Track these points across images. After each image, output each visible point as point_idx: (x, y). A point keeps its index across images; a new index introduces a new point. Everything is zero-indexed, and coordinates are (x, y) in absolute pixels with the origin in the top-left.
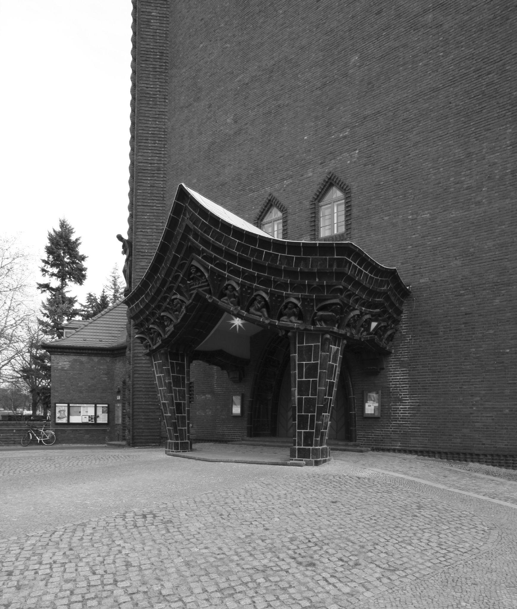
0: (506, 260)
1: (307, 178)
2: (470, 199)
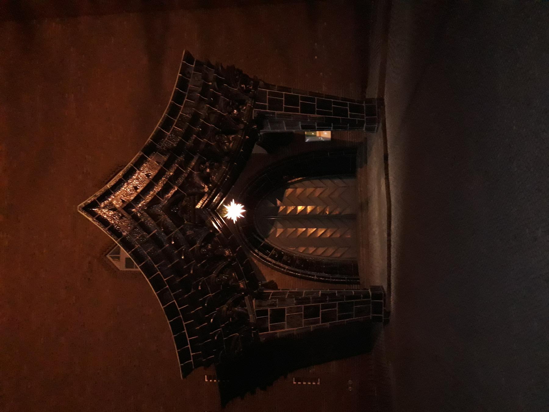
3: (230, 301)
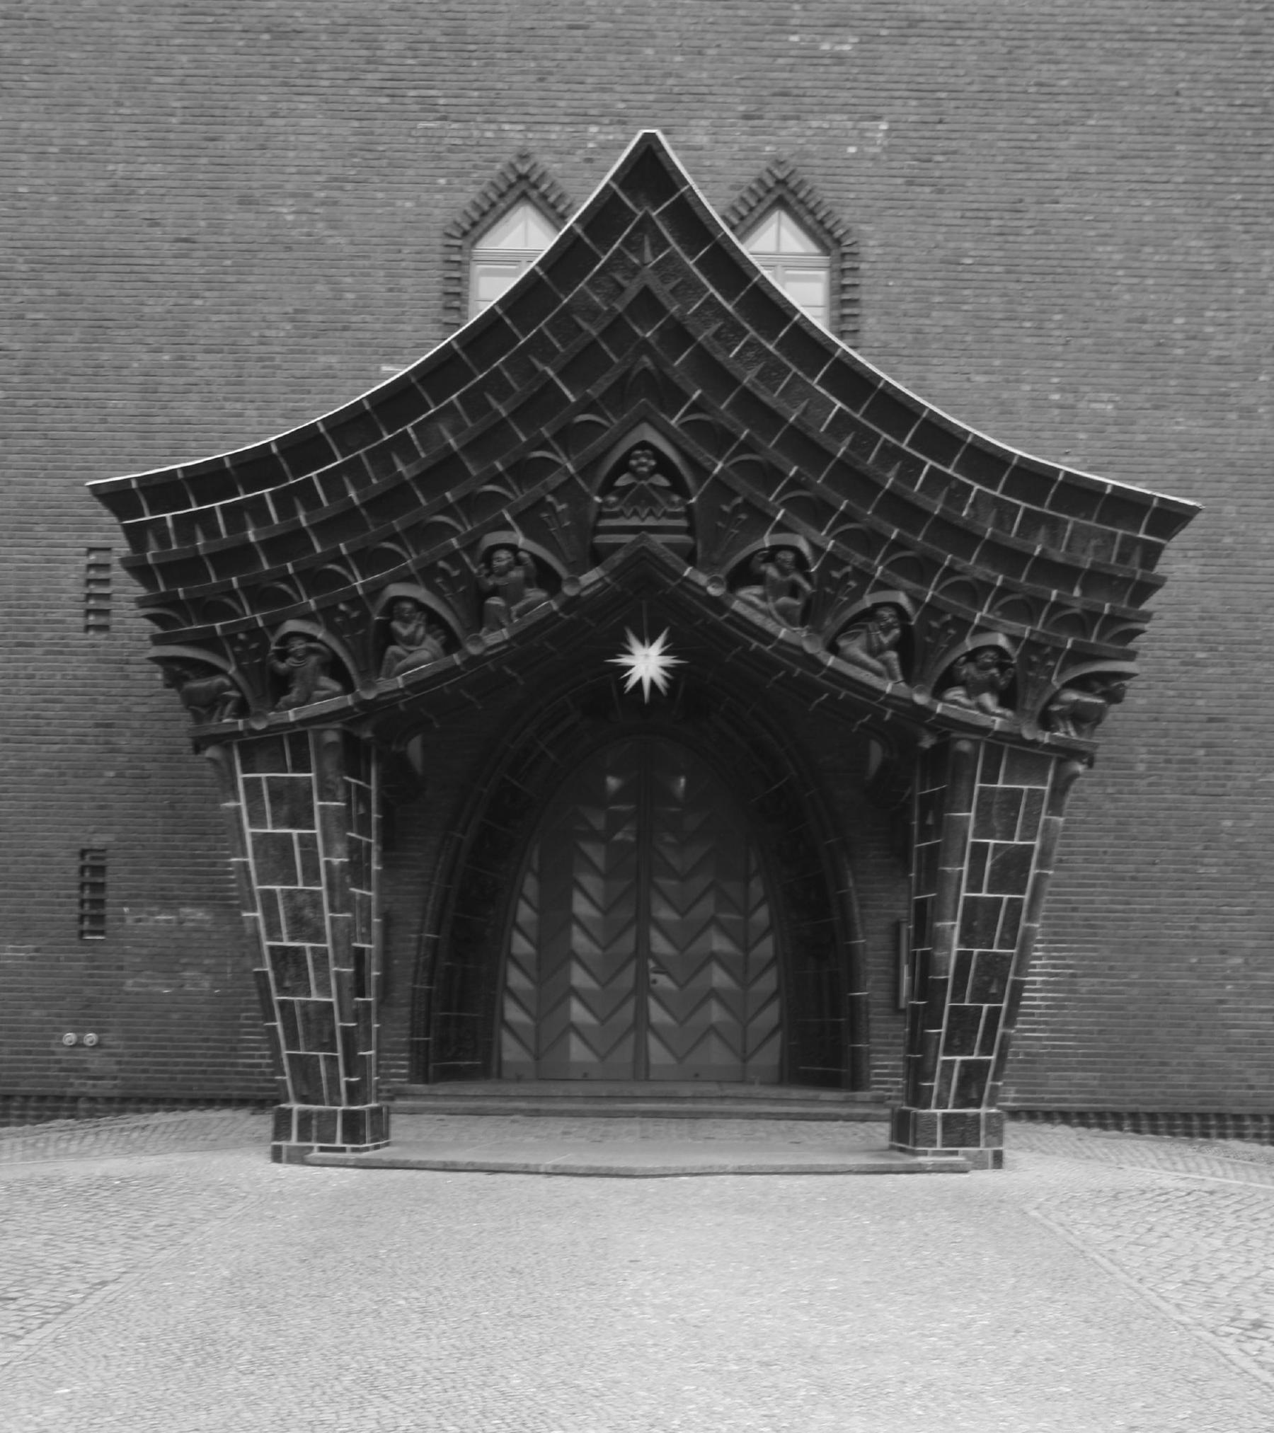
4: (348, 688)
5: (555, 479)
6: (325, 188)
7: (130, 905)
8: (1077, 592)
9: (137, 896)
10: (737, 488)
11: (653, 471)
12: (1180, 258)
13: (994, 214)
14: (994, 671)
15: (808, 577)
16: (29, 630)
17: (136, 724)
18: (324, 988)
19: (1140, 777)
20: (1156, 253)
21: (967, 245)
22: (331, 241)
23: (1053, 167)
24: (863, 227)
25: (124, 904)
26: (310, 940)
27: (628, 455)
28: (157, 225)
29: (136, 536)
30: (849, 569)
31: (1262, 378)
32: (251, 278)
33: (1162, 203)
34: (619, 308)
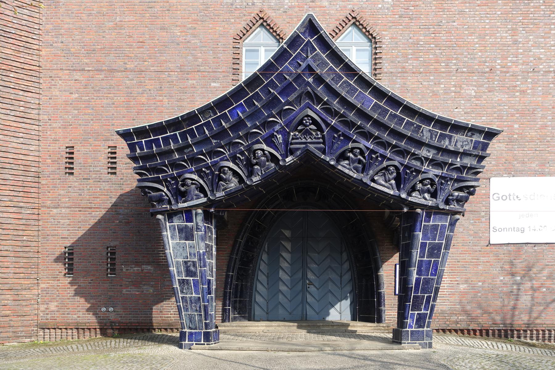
0: (547, 152)
1: (321, 7)
2: (515, 86)
3: (201, 182)
4: (206, 195)
5: (277, 128)
6: (190, 24)
7: (125, 265)
8: (459, 160)
9: (127, 262)
10: (339, 129)
11: (310, 124)
12: (499, 40)
13: (431, 27)
14: (429, 186)
15: (364, 157)
16: (88, 174)
17: (126, 205)
18: (197, 292)
19: (483, 217)
20: (490, 38)
21: (421, 38)
22: (193, 42)
23: (453, 10)
24: (384, 33)
25: (122, 265)
26: (192, 277)
27: (302, 119)
28: (132, 37)
29: (132, 147)
30: (378, 154)
31: (529, 80)
32: (165, 55)
33: (493, 21)
34: (299, 71)
